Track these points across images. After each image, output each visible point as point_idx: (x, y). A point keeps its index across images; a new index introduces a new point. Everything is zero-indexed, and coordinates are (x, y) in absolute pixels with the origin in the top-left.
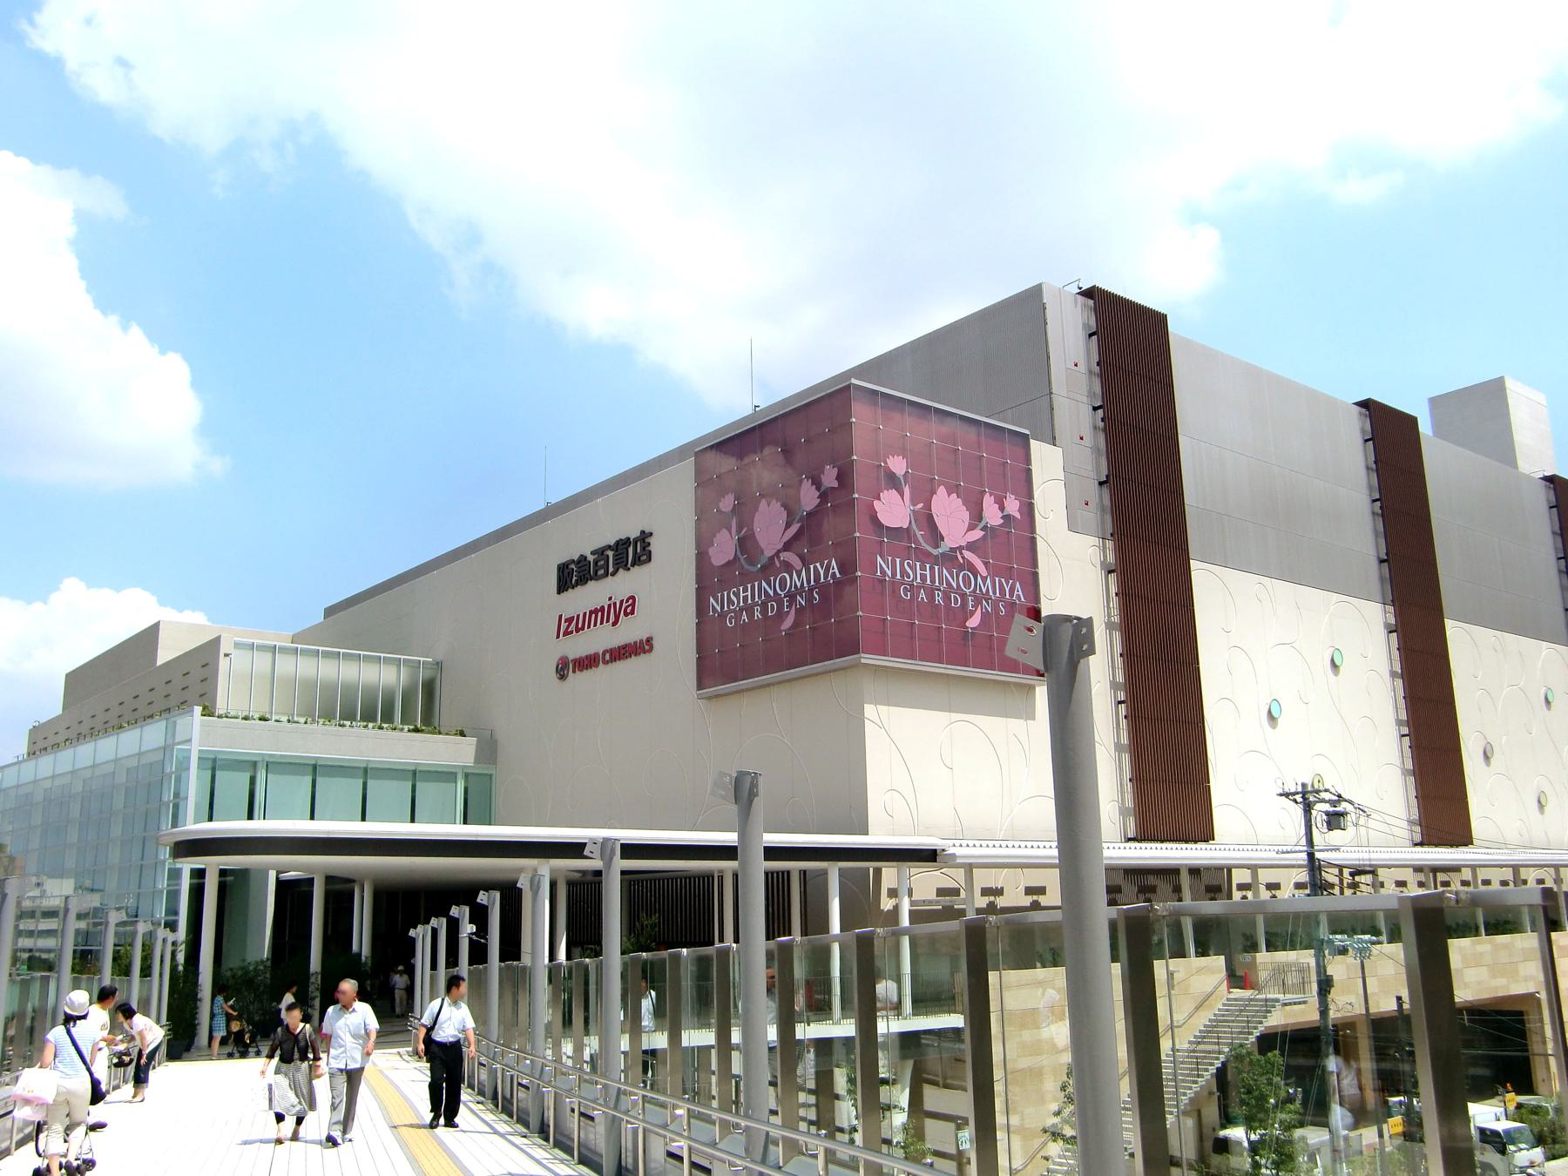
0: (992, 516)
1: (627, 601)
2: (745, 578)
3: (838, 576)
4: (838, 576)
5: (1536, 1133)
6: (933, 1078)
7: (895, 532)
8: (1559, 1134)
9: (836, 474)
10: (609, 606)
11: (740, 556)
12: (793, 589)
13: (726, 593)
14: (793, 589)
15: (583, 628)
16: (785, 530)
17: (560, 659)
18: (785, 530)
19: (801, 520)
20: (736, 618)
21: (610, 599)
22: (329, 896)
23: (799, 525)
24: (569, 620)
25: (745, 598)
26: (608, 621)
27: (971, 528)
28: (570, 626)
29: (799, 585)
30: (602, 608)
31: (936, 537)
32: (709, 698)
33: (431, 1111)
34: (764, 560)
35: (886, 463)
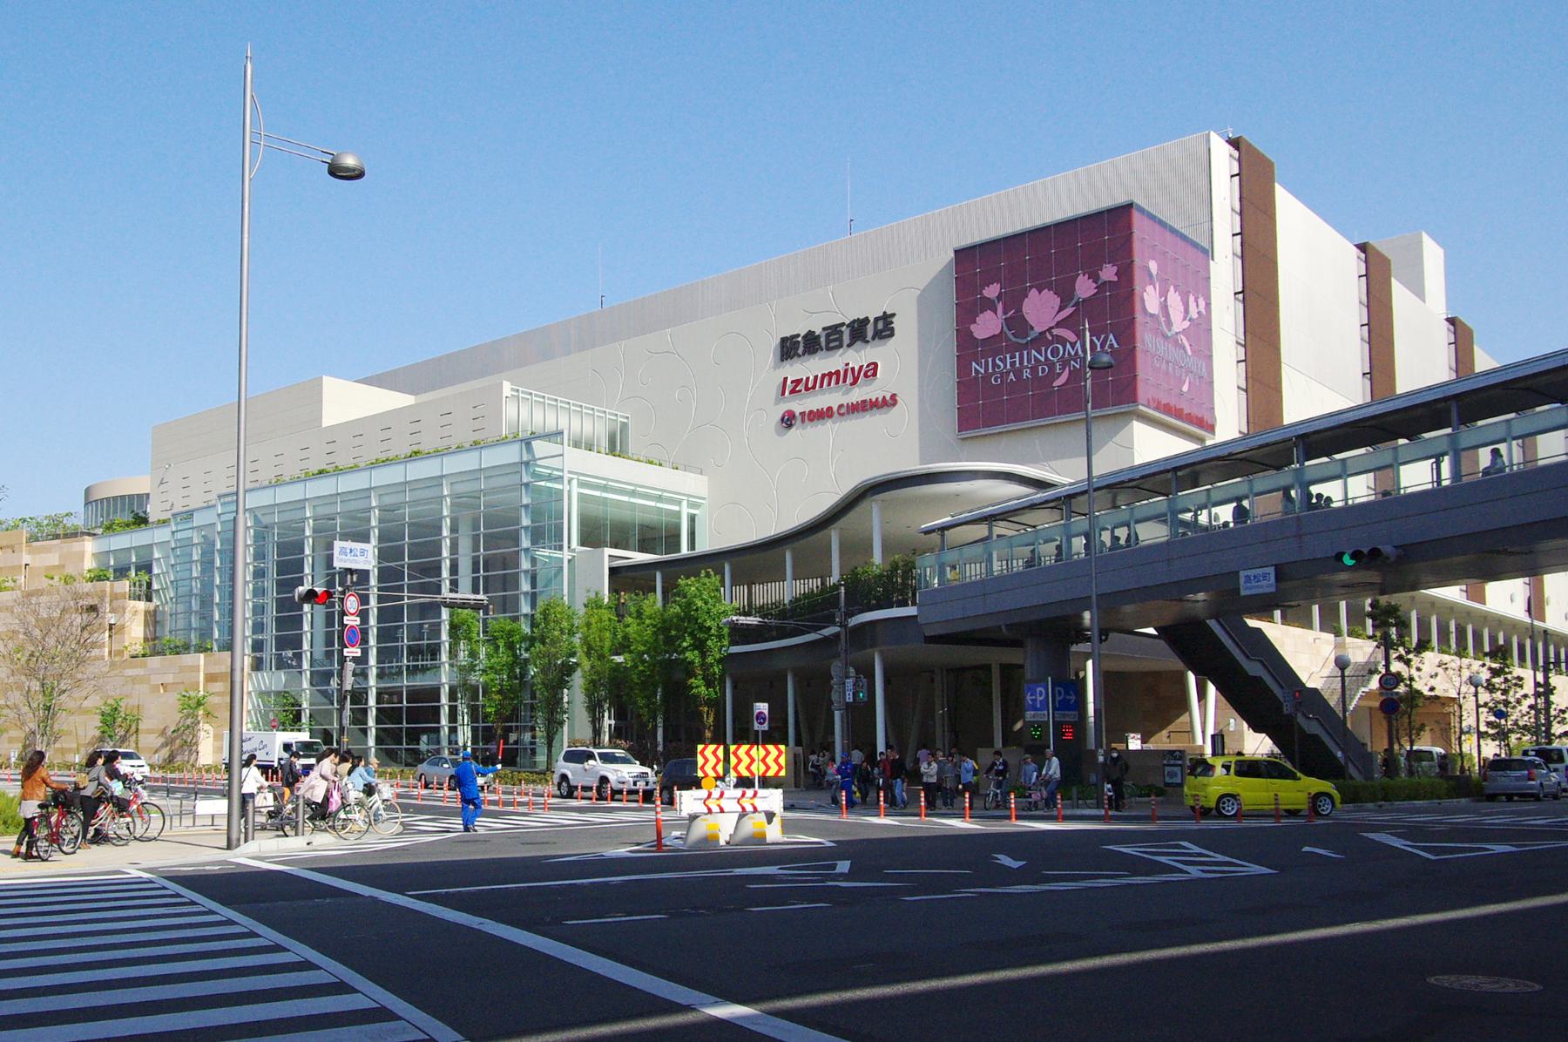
0: (1193, 313)
1: (868, 366)
2: (1013, 348)
3: (1116, 346)
4: (1116, 346)
5: (1188, 713)
6: (244, 574)
7: (1152, 315)
8: (68, 531)
9: (1115, 271)
10: (846, 371)
11: (1007, 332)
12: (1066, 356)
13: (990, 360)
14: (1066, 356)
15: (814, 387)
16: (1058, 313)
17: (786, 412)
18: (1058, 313)
19: (1077, 304)
20: (1002, 377)
21: (847, 364)
22: (479, 590)
23: (1074, 308)
24: (798, 382)
25: (1013, 364)
26: (845, 381)
27: (1184, 320)
28: (797, 387)
29: (1073, 353)
30: (837, 373)
31: (1169, 324)
32: (963, 439)
33: (688, 814)
34: (1033, 335)
35: (1031, 287)
